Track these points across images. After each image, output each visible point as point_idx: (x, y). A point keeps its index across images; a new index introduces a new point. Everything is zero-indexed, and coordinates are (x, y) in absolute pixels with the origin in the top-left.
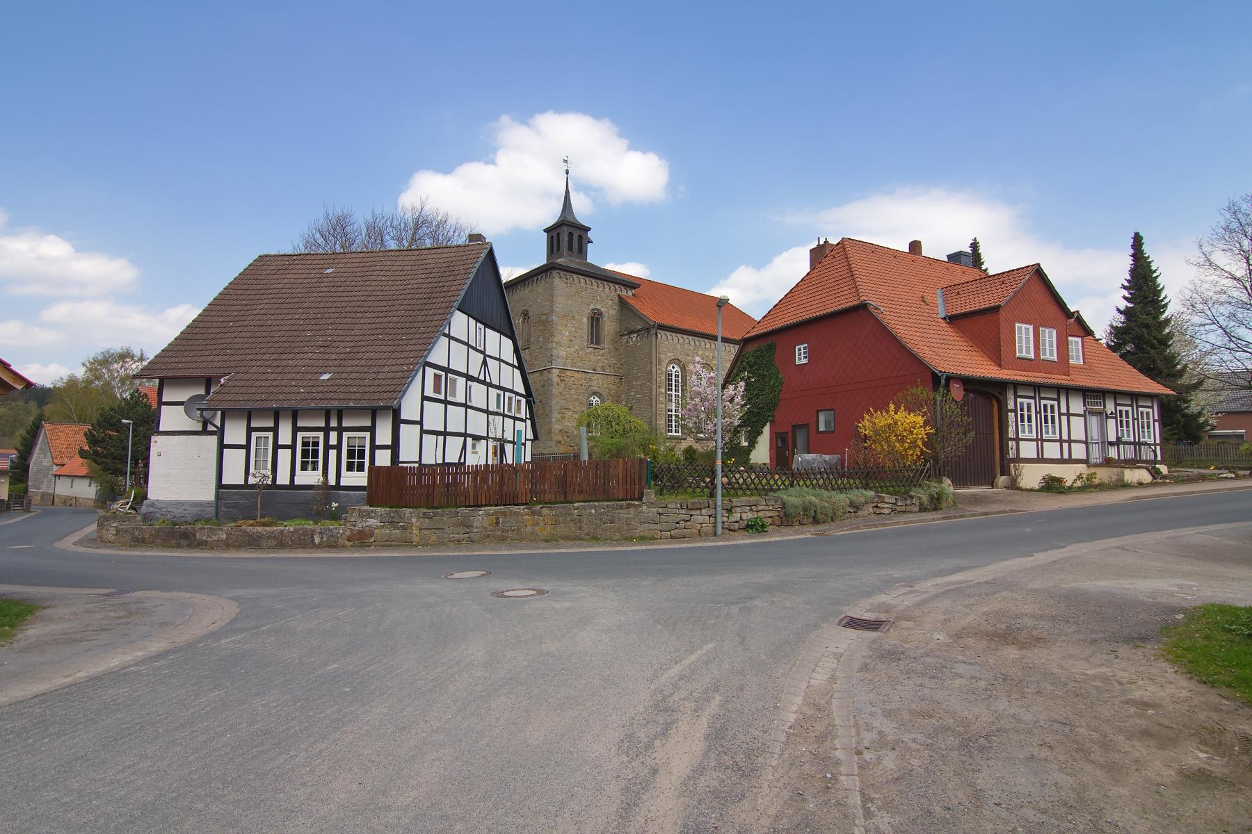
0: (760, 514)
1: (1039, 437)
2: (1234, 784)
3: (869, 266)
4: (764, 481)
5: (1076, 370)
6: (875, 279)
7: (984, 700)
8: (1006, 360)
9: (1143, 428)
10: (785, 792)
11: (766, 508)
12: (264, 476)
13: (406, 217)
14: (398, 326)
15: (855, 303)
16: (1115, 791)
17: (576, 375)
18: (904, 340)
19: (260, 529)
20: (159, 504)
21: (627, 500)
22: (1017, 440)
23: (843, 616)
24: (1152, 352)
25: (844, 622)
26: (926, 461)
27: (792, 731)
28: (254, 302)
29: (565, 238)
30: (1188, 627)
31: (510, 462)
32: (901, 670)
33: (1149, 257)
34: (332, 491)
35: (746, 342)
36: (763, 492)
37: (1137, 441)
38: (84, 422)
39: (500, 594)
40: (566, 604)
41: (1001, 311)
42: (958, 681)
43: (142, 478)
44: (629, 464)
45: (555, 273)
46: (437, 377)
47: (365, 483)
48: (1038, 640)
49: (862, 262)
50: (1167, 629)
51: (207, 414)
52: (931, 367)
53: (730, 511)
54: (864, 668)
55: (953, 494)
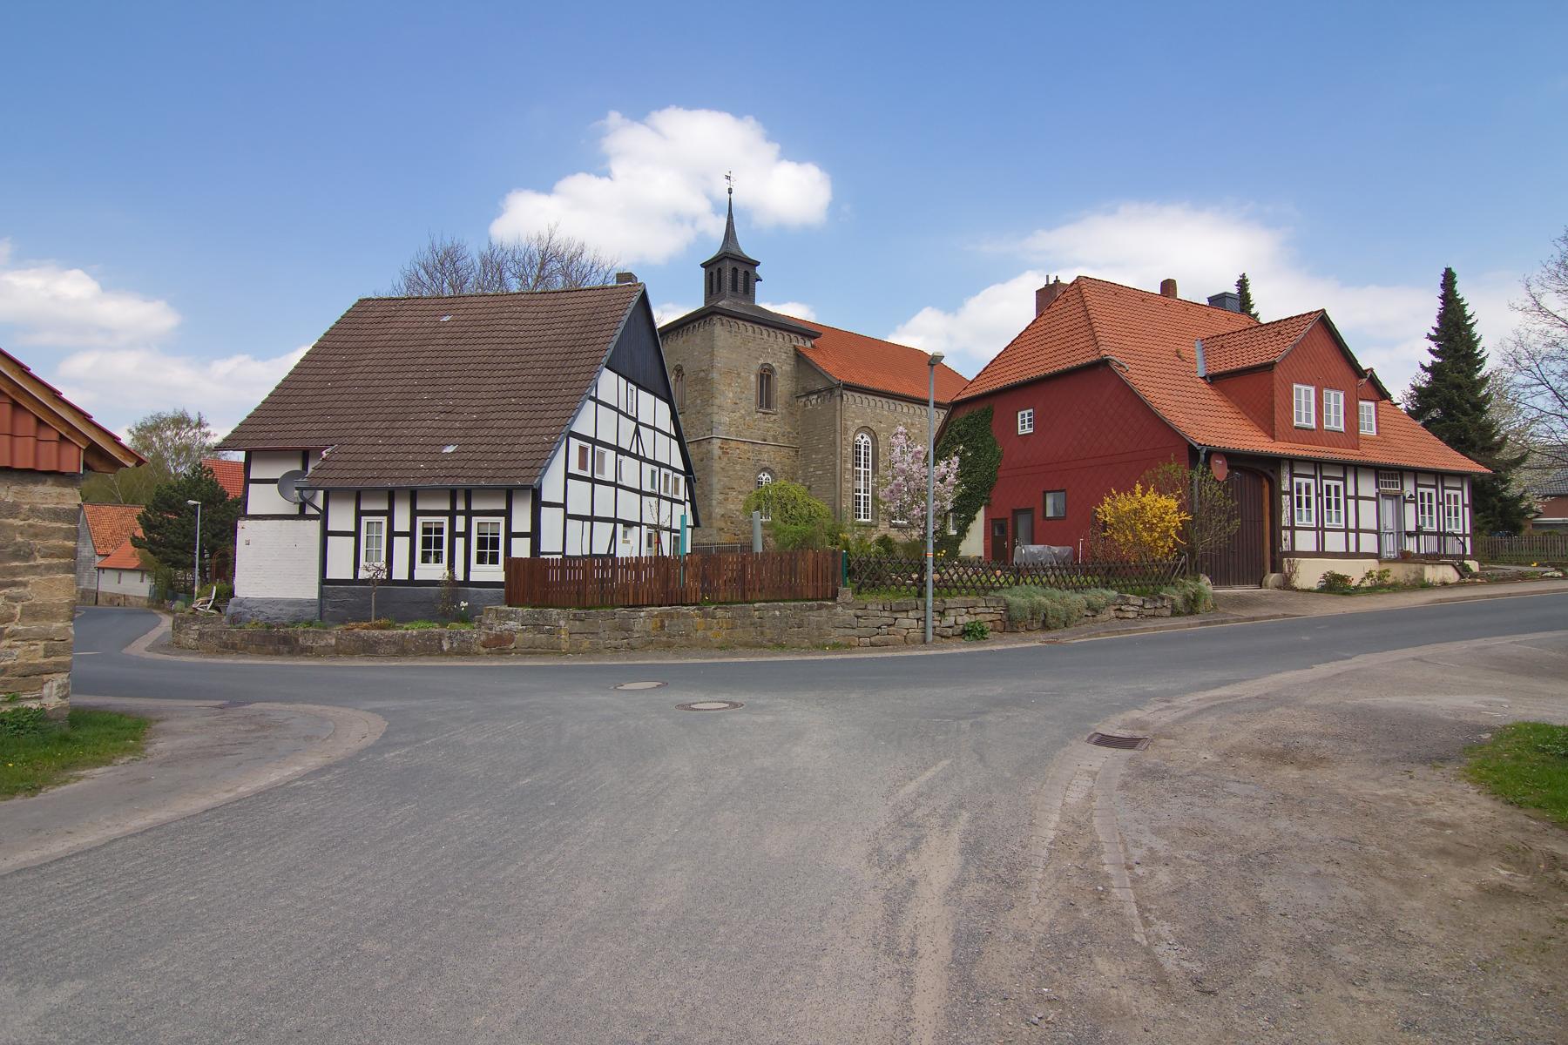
0: (979, 618)
1: (1320, 526)
2: (1537, 898)
3: (1112, 312)
4: (984, 578)
5: (1367, 442)
6: (1119, 329)
7: (1263, 818)
8: (1281, 430)
9: (1449, 514)
10: (1056, 902)
11: (987, 610)
12: (379, 569)
13: (531, 249)
14: (535, 386)
15: (1094, 359)
16: (1409, 904)
17: (742, 446)
18: (1155, 405)
19: (376, 633)
20: (248, 603)
21: (817, 600)
22: (1293, 529)
23: (1092, 733)
24: (1464, 419)
25: (1093, 740)
26: (1180, 555)
27: (1053, 847)
28: (355, 357)
29: (728, 275)
30: (1495, 747)
31: (666, 553)
32: (1167, 789)
33: (1462, 299)
34: (459, 588)
35: (955, 406)
36: (982, 592)
37: (1441, 530)
38: (134, 502)
39: (687, 707)
40: (769, 718)
41: (1276, 369)
42: (1232, 801)
43: (223, 567)
44: (821, 556)
45: (716, 318)
46: (583, 450)
47: (501, 577)
48: (1321, 760)
49: (1102, 306)
50: (1469, 749)
51: (307, 494)
52: (1188, 439)
53: (942, 613)
54: (1124, 786)
55: (1214, 595)
